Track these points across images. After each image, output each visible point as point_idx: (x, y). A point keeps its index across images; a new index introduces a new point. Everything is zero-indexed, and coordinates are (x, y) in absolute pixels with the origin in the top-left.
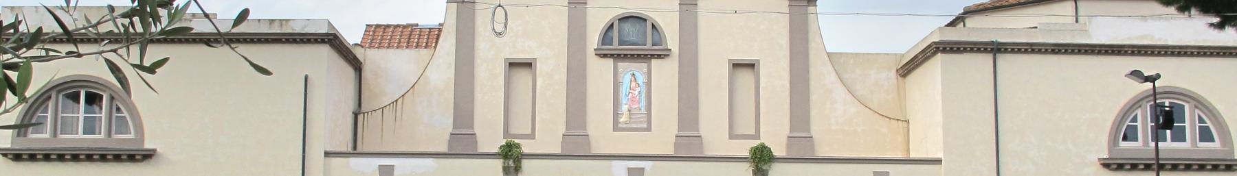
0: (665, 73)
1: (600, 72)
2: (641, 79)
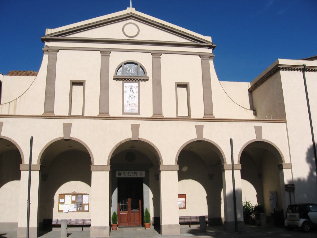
0: (147, 87)
1: (115, 86)
2: (135, 90)
